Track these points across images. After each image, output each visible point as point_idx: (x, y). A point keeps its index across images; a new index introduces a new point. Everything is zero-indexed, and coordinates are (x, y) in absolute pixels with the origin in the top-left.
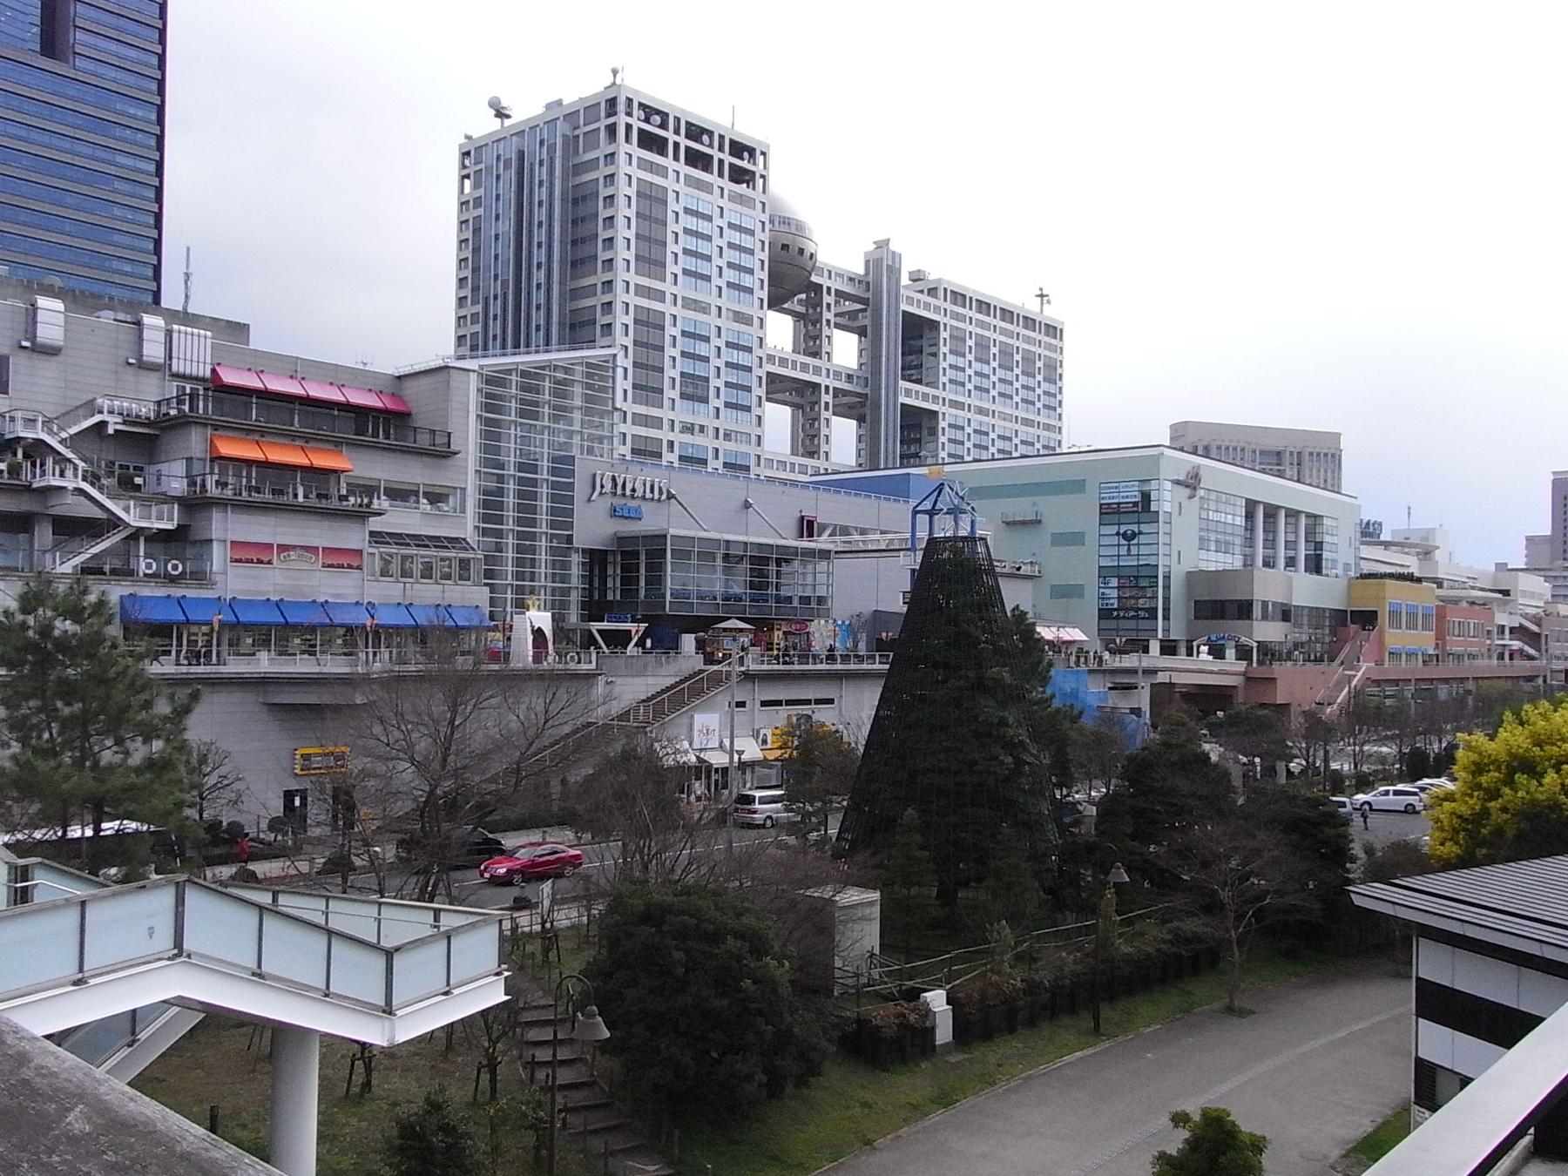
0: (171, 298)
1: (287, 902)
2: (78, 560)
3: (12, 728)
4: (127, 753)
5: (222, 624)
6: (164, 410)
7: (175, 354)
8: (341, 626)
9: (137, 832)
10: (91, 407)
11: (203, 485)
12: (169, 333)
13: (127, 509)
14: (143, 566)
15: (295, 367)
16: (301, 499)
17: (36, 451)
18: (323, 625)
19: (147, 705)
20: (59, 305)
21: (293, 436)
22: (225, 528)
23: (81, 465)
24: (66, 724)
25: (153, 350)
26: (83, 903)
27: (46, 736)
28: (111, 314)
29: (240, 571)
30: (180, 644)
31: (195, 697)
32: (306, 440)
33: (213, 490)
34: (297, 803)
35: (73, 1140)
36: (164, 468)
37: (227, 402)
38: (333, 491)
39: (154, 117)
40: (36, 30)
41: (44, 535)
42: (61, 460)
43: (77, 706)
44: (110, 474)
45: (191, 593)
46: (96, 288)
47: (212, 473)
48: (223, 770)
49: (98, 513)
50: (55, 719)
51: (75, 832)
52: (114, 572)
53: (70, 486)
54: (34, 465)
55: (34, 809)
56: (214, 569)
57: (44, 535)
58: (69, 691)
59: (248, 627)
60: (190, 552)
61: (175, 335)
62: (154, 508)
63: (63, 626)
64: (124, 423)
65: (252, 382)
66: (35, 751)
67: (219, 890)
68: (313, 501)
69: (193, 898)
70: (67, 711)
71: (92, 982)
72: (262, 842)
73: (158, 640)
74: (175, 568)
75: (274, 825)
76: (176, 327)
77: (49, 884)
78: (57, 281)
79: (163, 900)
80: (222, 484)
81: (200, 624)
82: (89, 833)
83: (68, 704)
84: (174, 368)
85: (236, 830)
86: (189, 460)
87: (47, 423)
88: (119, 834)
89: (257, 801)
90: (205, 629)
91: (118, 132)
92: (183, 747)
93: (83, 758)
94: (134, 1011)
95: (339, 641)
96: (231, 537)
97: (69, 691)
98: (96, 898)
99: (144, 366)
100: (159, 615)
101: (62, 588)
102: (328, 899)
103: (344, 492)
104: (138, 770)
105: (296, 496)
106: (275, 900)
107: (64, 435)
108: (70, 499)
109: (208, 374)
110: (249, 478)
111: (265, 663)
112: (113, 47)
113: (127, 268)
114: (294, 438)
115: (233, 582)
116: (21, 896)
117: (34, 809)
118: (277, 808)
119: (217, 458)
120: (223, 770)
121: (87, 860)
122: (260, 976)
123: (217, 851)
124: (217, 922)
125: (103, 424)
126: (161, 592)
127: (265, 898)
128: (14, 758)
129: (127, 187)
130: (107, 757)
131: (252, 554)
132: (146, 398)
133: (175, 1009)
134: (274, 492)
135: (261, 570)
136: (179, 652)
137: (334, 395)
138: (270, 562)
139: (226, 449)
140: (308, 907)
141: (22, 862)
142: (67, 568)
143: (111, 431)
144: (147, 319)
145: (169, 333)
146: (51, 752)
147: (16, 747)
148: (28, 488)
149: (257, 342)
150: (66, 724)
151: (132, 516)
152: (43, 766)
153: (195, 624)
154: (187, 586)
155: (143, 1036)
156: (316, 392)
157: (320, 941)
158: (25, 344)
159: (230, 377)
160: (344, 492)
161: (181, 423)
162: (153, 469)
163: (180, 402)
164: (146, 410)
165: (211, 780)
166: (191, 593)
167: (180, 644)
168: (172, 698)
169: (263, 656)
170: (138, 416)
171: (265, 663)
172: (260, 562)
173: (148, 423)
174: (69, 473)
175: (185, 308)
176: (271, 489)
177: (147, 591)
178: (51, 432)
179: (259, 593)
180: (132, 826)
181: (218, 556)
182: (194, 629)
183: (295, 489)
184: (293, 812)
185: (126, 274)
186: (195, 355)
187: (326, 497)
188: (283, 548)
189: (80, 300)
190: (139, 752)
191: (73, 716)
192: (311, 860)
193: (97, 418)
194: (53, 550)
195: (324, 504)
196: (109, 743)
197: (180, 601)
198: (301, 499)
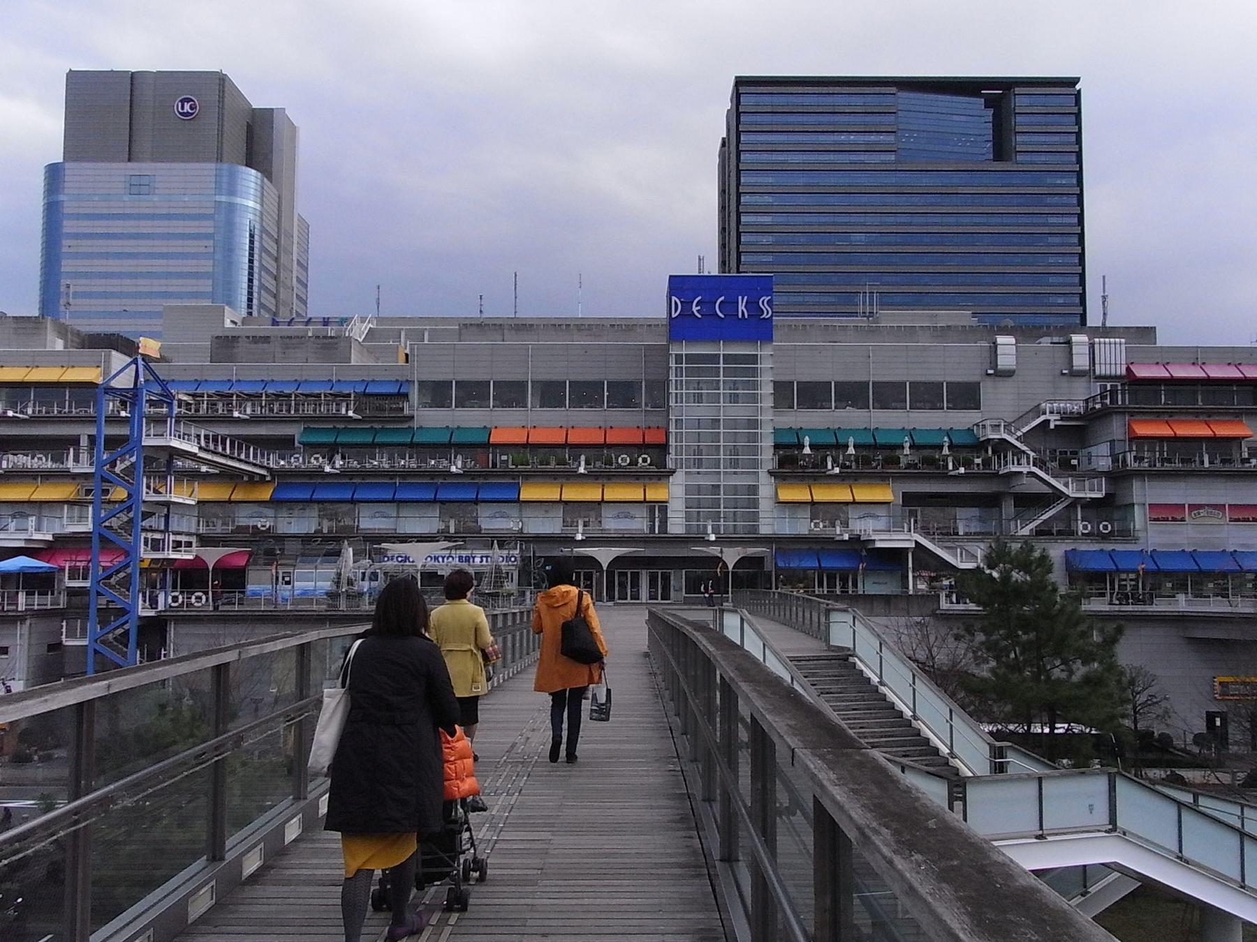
0: (1093, 320)
1: (1205, 803)
2: (1032, 526)
3: (988, 649)
4: (1071, 673)
5: (1146, 572)
6: (1091, 405)
7: (1097, 361)
8: (1249, 571)
9: (1082, 733)
10: (1037, 411)
11: (1124, 460)
12: (1092, 346)
13: (1066, 485)
14: (1081, 527)
15: (1196, 355)
16: (1207, 465)
17: (1002, 447)
18: (1232, 572)
19: (1084, 635)
20: (1012, 340)
21: (1197, 413)
22: (1143, 494)
23: (1032, 454)
24: (1026, 647)
25: (1081, 361)
26: (1040, 779)
27: (1012, 655)
28: (1048, 339)
29: (1156, 528)
30: (1113, 588)
31: (1120, 631)
32: (1207, 415)
33: (1132, 465)
34: (1218, 723)
35: (928, 830)
36: (1093, 450)
37: (1140, 392)
38: (1236, 456)
39: (1074, 181)
40: (989, 144)
41: (1009, 508)
42: (1018, 453)
43: (1032, 635)
44: (1053, 459)
45: (1120, 547)
46: (1038, 320)
47: (1130, 451)
48: (1151, 691)
49: (1046, 490)
50: (1018, 644)
51: (1037, 729)
52: (1060, 533)
53: (1025, 470)
54: (999, 458)
55: (1008, 708)
56: (1137, 527)
57: (1009, 508)
58: (1025, 623)
59: (1169, 574)
60: (1116, 515)
61: (1097, 347)
62: (1087, 483)
63: (1016, 576)
64: (1062, 419)
65: (1160, 373)
66: (1008, 666)
67: (1150, 787)
68: (1218, 466)
69: (1122, 788)
70: (1025, 637)
71: (1050, 838)
72: (1189, 753)
73: (1096, 585)
74: (1106, 527)
75: (1198, 739)
76: (1097, 340)
77: (1017, 763)
78: (1010, 323)
79: (1098, 785)
80: (1138, 459)
81: (1128, 572)
82: (1047, 730)
83: (1025, 633)
84: (1098, 372)
85: (1165, 741)
86: (1112, 442)
87: (1007, 427)
88: (1068, 734)
89: (1184, 718)
90: (1132, 576)
91: (1049, 200)
92: (1111, 667)
93: (1039, 674)
94: (1085, 866)
95: (1250, 585)
96: (1149, 501)
97: (1025, 623)
98: (1049, 777)
99: (1075, 374)
100: (1094, 565)
101: (1015, 546)
102: (1242, 806)
103: (1246, 455)
104: (1078, 686)
105: (1202, 462)
106: (1196, 800)
107: (1019, 434)
108: (1025, 480)
109: (1124, 372)
110: (1161, 452)
111: (1182, 604)
112: (1043, 138)
113: (1061, 301)
114: (1197, 415)
115: (1153, 537)
116: (999, 768)
117: (1008, 708)
118: (1200, 726)
119: (1134, 439)
120: (1151, 691)
121: (1051, 751)
122: (1180, 858)
123: (1150, 756)
124: (1137, 806)
125: (1048, 421)
126: (1095, 547)
127: (1187, 798)
128: (992, 670)
129: (1057, 240)
130: (1057, 673)
131: (1166, 513)
132: (1076, 398)
133: (1116, 875)
134: (1183, 461)
135: (1170, 527)
136: (1112, 594)
137: (1233, 373)
138: (1183, 520)
139: (1142, 430)
140: (1228, 812)
141: (998, 744)
142: (1025, 531)
143: (1052, 426)
144: (1076, 338)
145: (1092, 346)
146: (1016, 667)
147: (993, 664)
148: (996, 475)
149: (1162, 340)
150: (1026, 647)
151: (1071, 491)
152: (1015, 677)
153: (1124, 572)
154: (1116, 541)
155: (1092, 890)
156: (1215, 372)
157: (1233, 841)
158: (990, 372)
159: (1141, 372)
160: (1246, 455)
161: (1105, 414)
162: (1085, 451)
163: (1103, 397)
164: (1077, 407)
165: (1142, 698)
166: (1120, 547)
167: (1113, 588)
168: (1101, 631)
169: (1181, 597)
170: (1072, 413)
171: (1182, 604)
172: (1174, 519)
173: (1079, 417)
174: (1024, 461)
175: (1104, 323)
176: (1180, 459)
177: (1084, 547)
178: (1010, 433)
179: (1175, 545)
180: (1077, 728)
181: (1139, 517)
182: (1124, 576)
183: (1201, 456)
184: (1215, 733)
185: (1059, 305)
186: (1113, 358)
187: (1230, 461)
188: (1193, 507)
189: (1025, 333)
190: (1080, 670)
191: (1030, 642)
192: (1234, 774)
193: (1042, 418)
194: (1015, 519)
195: (1227, 467)
196: (1058, 663)
197: (1111, 554)
198: (1207, 465)
